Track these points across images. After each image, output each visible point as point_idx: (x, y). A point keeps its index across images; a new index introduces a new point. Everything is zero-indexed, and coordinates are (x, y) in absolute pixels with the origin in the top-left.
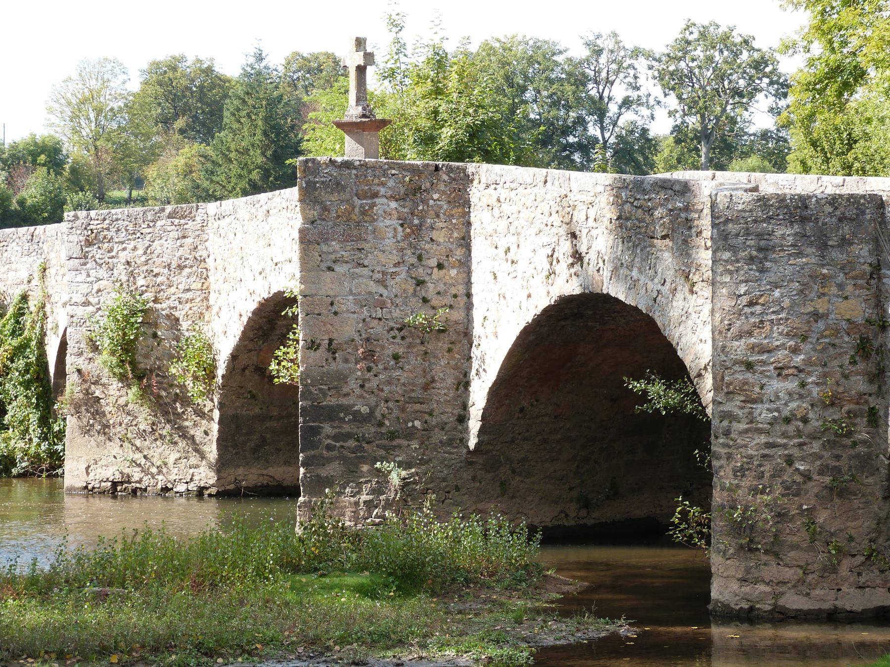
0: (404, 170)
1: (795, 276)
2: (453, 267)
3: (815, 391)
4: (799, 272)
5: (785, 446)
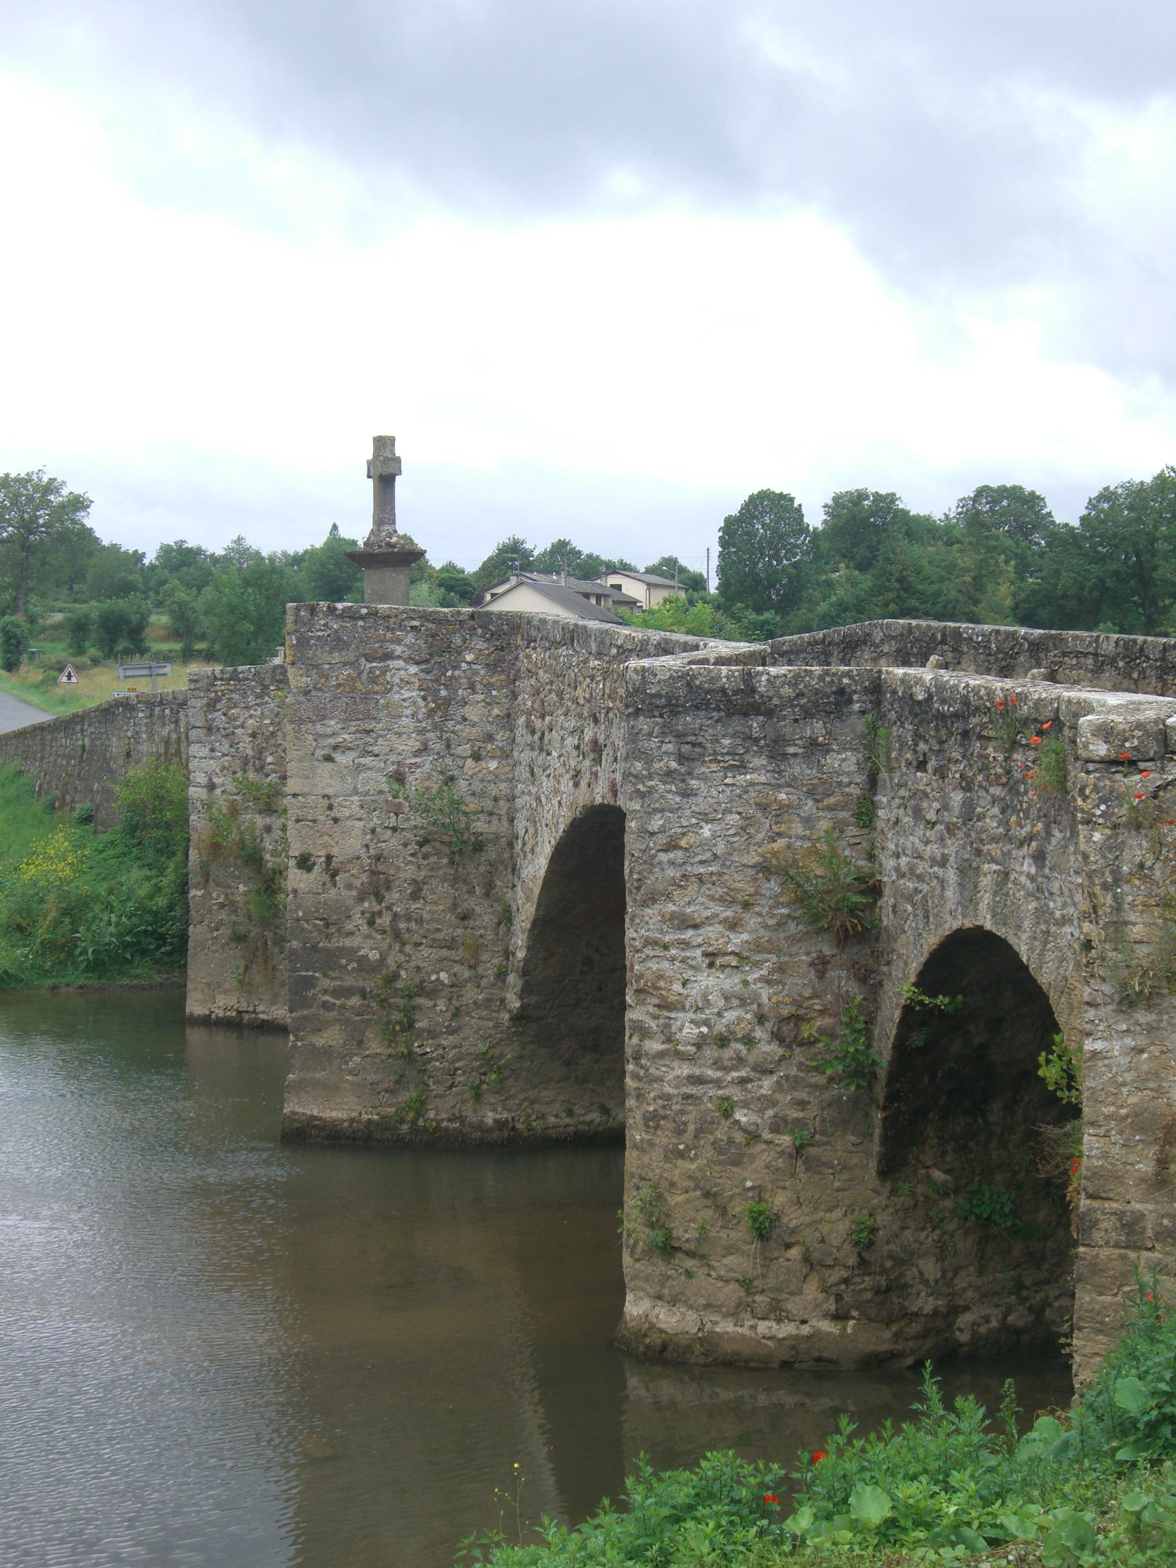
0: (428, 621)
1: (735, 804)
2: (493, 758)
3: (765, 993)
4: (740, 797)
5: (718, 1083)
